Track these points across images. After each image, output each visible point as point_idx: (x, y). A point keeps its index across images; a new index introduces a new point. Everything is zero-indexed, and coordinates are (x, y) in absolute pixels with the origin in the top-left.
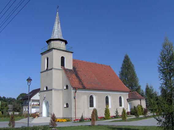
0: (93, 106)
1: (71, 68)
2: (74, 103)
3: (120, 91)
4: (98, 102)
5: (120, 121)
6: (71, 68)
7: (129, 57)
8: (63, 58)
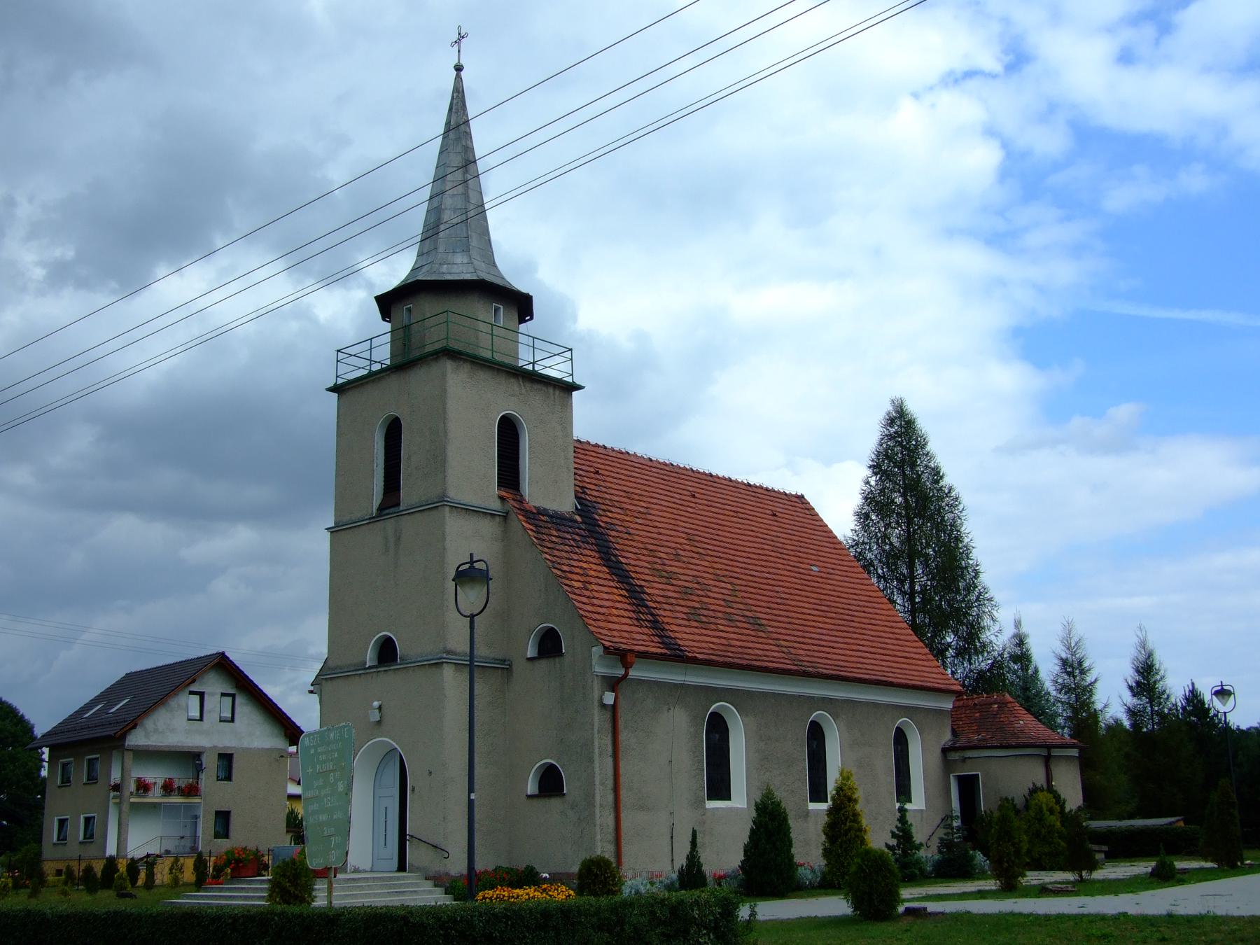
0: (710, 800)
1: (565, 504)
2: (610, 761)
3: (891, 684)
4: (760, 760)
5: (981, 895)
6: (565, 504)
7: (924, 425)
8: (509, 431)
